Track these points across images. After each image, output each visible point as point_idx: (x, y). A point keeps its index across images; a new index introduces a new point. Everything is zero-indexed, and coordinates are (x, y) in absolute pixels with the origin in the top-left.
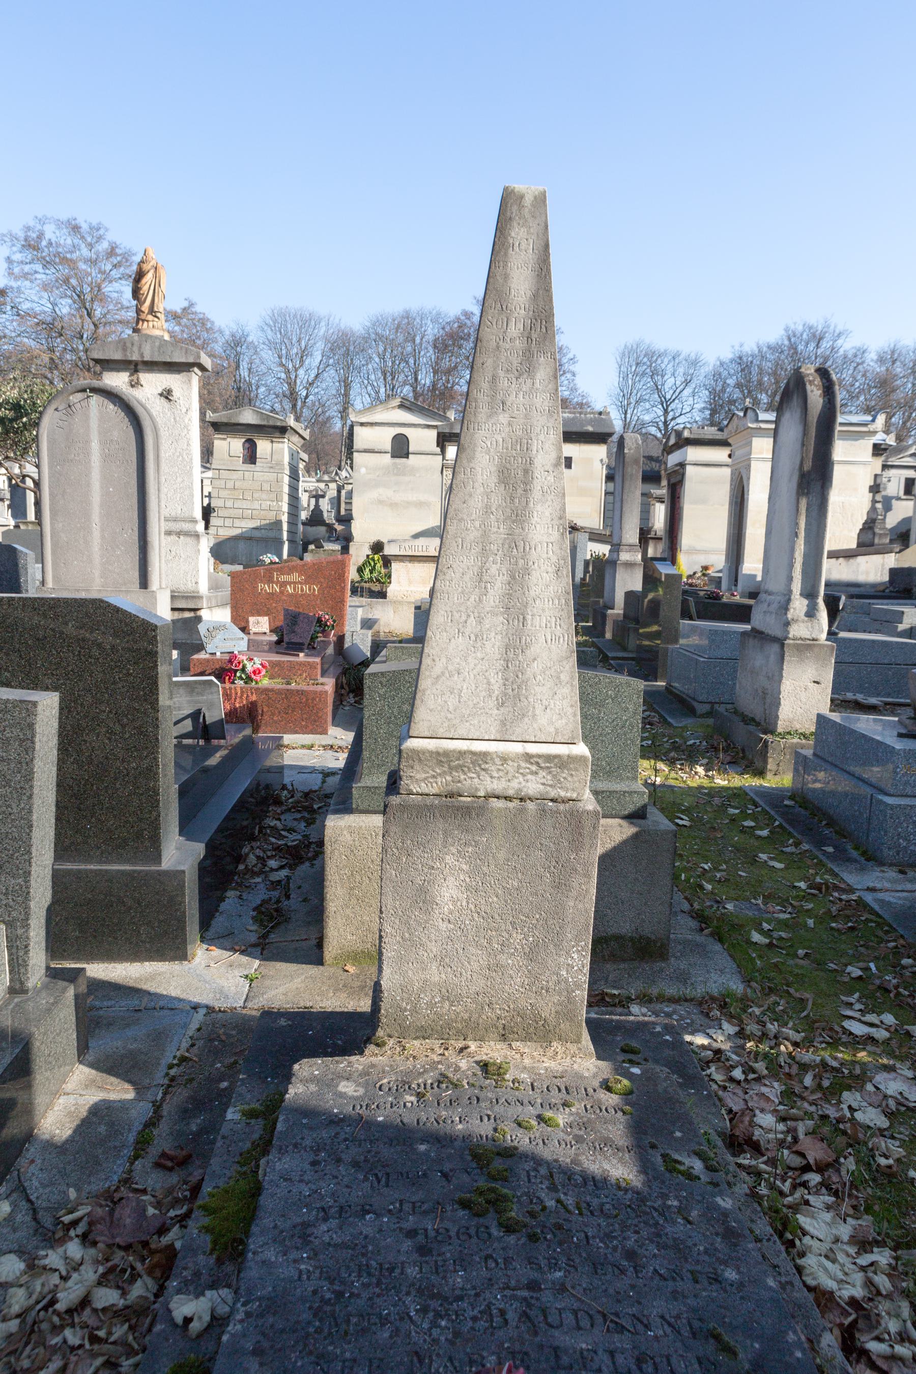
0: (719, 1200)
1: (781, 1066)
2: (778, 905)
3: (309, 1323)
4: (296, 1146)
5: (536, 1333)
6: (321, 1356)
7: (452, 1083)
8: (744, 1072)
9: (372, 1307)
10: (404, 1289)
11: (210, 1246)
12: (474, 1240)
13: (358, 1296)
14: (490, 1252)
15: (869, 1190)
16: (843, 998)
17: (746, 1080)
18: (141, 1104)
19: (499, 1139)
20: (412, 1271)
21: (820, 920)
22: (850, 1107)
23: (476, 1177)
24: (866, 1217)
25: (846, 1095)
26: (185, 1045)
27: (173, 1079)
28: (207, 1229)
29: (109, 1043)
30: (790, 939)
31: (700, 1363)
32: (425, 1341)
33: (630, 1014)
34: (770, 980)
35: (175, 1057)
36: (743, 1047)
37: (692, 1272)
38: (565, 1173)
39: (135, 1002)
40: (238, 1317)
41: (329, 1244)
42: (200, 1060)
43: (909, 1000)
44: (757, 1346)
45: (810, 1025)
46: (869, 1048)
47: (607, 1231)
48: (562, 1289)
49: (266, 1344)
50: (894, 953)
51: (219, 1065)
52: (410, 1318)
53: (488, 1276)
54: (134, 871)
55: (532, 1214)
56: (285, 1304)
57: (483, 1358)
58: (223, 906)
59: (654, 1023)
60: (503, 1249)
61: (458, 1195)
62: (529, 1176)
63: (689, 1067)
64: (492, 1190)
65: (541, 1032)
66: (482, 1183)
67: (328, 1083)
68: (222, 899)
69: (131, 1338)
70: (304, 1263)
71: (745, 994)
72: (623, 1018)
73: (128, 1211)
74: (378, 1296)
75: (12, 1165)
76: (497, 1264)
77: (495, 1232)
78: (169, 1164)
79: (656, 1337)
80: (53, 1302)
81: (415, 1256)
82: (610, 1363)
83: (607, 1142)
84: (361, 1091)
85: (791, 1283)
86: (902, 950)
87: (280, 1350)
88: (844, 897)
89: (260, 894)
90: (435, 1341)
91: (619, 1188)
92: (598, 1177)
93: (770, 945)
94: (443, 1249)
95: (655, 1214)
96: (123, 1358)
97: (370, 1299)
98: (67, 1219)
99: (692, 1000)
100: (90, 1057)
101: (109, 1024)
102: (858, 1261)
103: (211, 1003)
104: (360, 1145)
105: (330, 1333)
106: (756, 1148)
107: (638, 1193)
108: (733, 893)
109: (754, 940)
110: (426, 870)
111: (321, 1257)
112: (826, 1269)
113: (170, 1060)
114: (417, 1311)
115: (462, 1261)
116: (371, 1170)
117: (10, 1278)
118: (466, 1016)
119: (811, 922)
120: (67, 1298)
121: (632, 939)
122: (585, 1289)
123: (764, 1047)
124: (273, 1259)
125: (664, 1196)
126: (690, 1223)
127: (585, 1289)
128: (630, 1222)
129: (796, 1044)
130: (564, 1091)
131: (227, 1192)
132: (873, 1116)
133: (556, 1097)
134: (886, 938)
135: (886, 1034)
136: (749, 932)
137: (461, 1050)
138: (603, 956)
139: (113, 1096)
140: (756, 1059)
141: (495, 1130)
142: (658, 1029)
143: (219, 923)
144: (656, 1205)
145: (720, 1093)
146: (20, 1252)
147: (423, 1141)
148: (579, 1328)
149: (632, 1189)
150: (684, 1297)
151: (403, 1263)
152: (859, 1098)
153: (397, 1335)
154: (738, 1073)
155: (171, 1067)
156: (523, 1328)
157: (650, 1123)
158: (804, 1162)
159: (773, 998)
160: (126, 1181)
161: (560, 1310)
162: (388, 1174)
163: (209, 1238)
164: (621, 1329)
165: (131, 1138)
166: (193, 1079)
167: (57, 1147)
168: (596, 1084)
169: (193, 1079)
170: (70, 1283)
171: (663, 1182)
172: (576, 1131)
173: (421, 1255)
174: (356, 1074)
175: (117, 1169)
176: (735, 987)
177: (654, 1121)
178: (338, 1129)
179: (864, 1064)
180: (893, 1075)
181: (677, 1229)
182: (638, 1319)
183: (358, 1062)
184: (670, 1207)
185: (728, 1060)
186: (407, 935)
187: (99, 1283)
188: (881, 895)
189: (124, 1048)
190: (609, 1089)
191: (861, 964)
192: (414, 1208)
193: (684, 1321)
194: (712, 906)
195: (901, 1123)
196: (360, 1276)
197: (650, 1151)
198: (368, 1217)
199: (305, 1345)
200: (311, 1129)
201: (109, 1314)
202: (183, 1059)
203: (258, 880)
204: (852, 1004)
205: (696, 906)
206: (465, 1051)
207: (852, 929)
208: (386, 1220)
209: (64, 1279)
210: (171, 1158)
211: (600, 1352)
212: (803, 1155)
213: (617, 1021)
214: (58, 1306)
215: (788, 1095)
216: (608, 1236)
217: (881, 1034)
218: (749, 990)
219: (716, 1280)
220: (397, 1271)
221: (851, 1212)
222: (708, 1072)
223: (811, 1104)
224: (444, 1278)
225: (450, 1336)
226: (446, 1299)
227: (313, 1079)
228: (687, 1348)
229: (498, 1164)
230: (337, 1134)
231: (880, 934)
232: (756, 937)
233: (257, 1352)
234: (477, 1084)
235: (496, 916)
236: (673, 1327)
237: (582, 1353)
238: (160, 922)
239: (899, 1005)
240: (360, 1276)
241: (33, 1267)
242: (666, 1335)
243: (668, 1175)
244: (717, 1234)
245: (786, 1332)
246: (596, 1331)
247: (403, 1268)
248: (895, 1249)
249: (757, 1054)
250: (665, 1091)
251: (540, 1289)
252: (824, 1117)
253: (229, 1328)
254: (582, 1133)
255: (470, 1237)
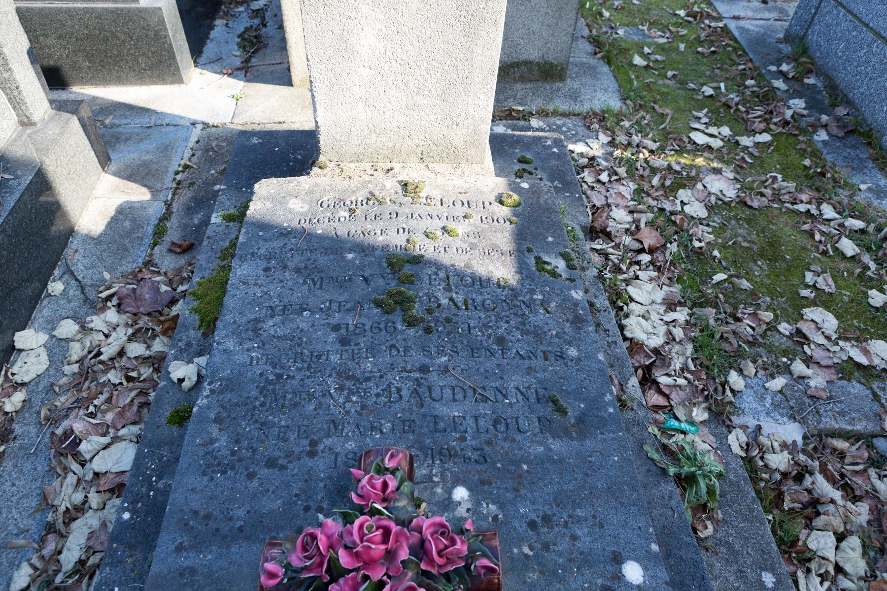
0: (573, 293)
1: (637, 169)
2: (659, 30)
3: (257, 398)
4: (253, 254)
5: (422, 406)
6: (263, 424)
7: (378, 201)
8: (609, 175)
9: (302, 386)
10: (328, 372)
11: (198, 323)
12: (384, 333)
13: (293, 377)
14: (394, 342)
15: (683, 266)
16: (695, 113)
17: (610, 181)
18: (156, 203)
19: (410, 249)
20: (335, 358)
21: (690, 45)
22: (682, 202)
23: (389, 281)
24: (676, 285)
25: (681, 192)
26: (187, 155)
27: (179, 183)
28: (195, 311)
29: (124, 155)
30: (664, 61)
31: (539, 421)
32: (340, 412)
33: (529, 128)
34: (641, 98)
35: (179, 165)
36: (611, 154)
37: (544, 352)
38: (458, 276)
39: (145, 120)
40: (205, 394)
41: (274, 336)
42: (199, 167)
43: (744, 115)
44: (582, 406)
45: (665, 136)
46: (706, 154)
47: (485, 322)
48: (445, 370)
49: (224, 414)
50: (741, 74)
51: (213, 172)
52: (331, 394)
53: (391, 362)
54: (117, 9)
55: (429, 311)
56: (239, 384)
57: (382, 425)
58: (213, 34)
59: (546, 138)
60: (404, 340)
61: (374, 296)
62: (430, 279)
63: (566, 173)
64: (400, 293)
65: (453, 155)
66: (393, 286)
67: (280, 200)
68: (212, 27)
69: (155, 376)
70: (254, 351)
71: (621, 111)
72: (523, 133)
73: (146, 289)
74: (308, 377)
75: (61, 254)
76: (399, 351)
77: (399, 326)
78: (178, 250)
79: (511, 404)
80: (99, 353)
81: (338, 346)
82: (474, 426)
83: (494, 248)
84: (306, 207)
85: (615, 343)
86: (748, 72)
87: (234, 419)
88: (713, 24)
89: (243, 22)
90: (348, 412)
91: (499, 286)
92: (484, 278)
93: (647, 67)
94: (359, 341)
95: (523, 307)
96: (151, 390)
97: (302, 380)
98: (104, 295)
99: (579, 114)
100: (113, 167)
101: (127, 140)
102: (664, 318)
103: (206, 120)
104: (302, 254)
105: (271, 407)
106: (608, 236)
107: (513, 290)
108: (625, 20)
109: (635, 63)
110: (344, 20)
111: (267, 346)
112: (641, 326)
113: (176, 168)
114: (336, 389)
115: (372, 350)
116: (310, 275)
117: (70, 336)
118: (391, 145)
119: (682, 47)
120: (108, 352)
121: (538, 64)
122: (462, 370)
123: (627, 154)
124: (232, 348)
125: (532, 292)
126: (548, 312)
127: (462, 370)
128: (503, 313)
129: (652, 152)
130: (466, 204)
131: (210, 281)
132: (697, 209)
133: (459, 211)
134: (737, 61)
135: (721, 143)
136: (632, 56)
137: (388, 171)
138: (514, 78)
139: (134, 198)
140: (620, 163)
141: (408, 241)
142: (549, 143)
143: (210, 49)
144: (525, 299)
145: (589, 192)
146: (75, 318)
147: (350, 250)
148: (455, 400)
149: (508, 286)
150: (537, 372)
151: (328, 352)
152: (690, 195)
153: (320, 408)
154: (604, 177)
155: (177, 173)
156: (413, 401)
157: (531, 229)
158: (641, 247)
159: (642, 113)
160: (148, 263)
161: (442, 387)
162: (322, 278)
163: (197, 317)
164: (486, 399)
165: (150, 230)
166: (194, 183)
167: (94, 239)
168: (492, 198)
169: (194, 183)
170: (110, 340)
171: (533, 280)
172: (471, 239)
173: (343, 345)
174: (303, 193)
175: (140, 255)
176: (613, 104)
177: (533, 228)
178: (286, 240)
179: (699, 167)
180: (719, 176)
181: (539, 318)
182: (499, 391)
183: (303, 182)
184: (535, 300)
185: (598, 165)
186: (334, 81)
187: (130, 340)
188: (742, 23)
189: (139, 159)
190: (501, 203)
191: (714, 85)
192: (340, 306)
193: (533, 390)
194: (606, 33)
195: (716, 214)
196: (295, 362)
197: (527, 254)
198: (305, 313)
199: (253, 415)
200: (265, 240)
201: (140, 361)
202: (186, 167)
203: (241, 9)
204: (700, 118)
205: (594, 32)
206: (391, 172)
207: (714, 52)
208: (318, 316)
209: (107, 336)
210: (180, 246)
211: (467, 418)
212: (641, 242)
213: (518, 136)
214: (102, 358)
215: (639, 193)
216: (486, 326)
217: (716, 143)
218: (624, 107)
219: (561, 357)
220: (324, 358)
221: (667, 282)
222: (582, 175)
223: (654, 199)
224: (358, 363)
225: (358, 409)
226: (358, 380)
227: (270, 197)
228: (532, 411)
229: (407, 270)
230: (285, 244)
231: (734, 57)
232: (638, 60)
233: (218, 420)
234: (398, 201)
235: (412, 63)
236: (524, 395)
237: (454, 419)
238: (153, 53)
239: (736, 119)
240: (295, 362)
241: (85, 329)
242: (518, 401)
243: (537, 274)
244: (567, 321)
245: (604, 395)
246: (467, 402)
247: (328, 355)
248: (691, 309)
249: (622, 159)
250: (545, 202)
251: (429, 371)
252: (662, 210)
253: (198, 402)
254: (476, 241)
255: (381, 330)
